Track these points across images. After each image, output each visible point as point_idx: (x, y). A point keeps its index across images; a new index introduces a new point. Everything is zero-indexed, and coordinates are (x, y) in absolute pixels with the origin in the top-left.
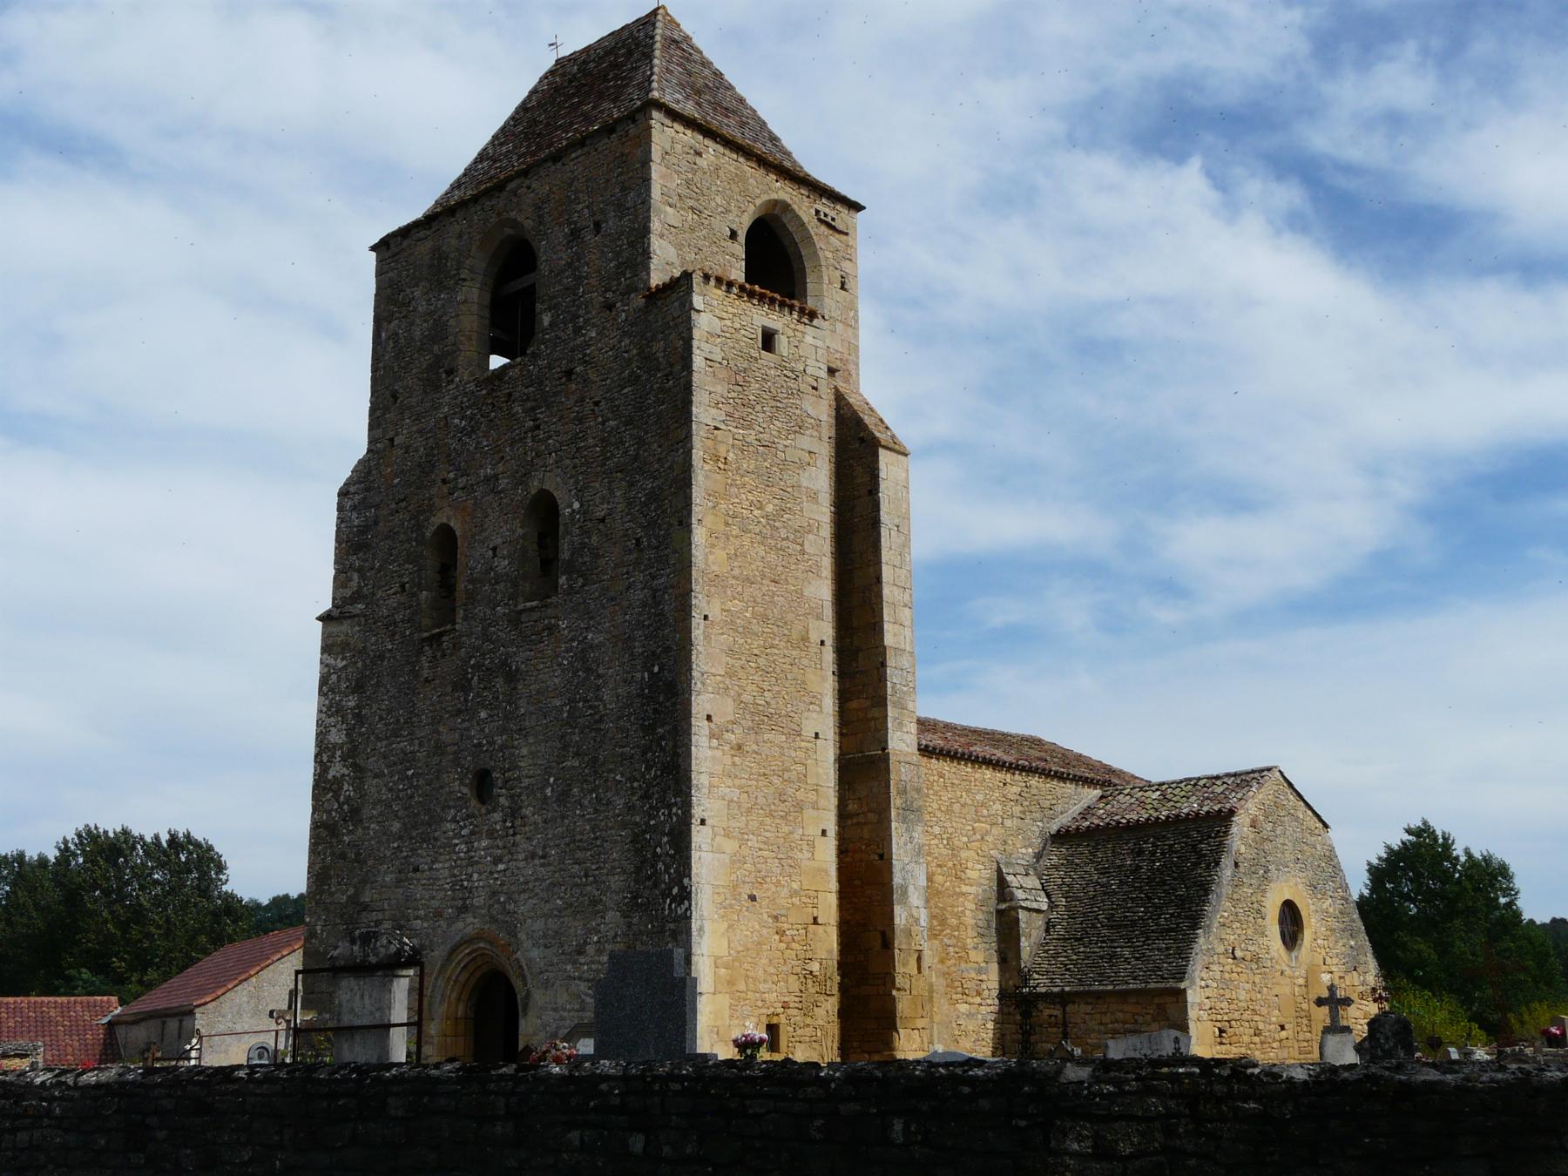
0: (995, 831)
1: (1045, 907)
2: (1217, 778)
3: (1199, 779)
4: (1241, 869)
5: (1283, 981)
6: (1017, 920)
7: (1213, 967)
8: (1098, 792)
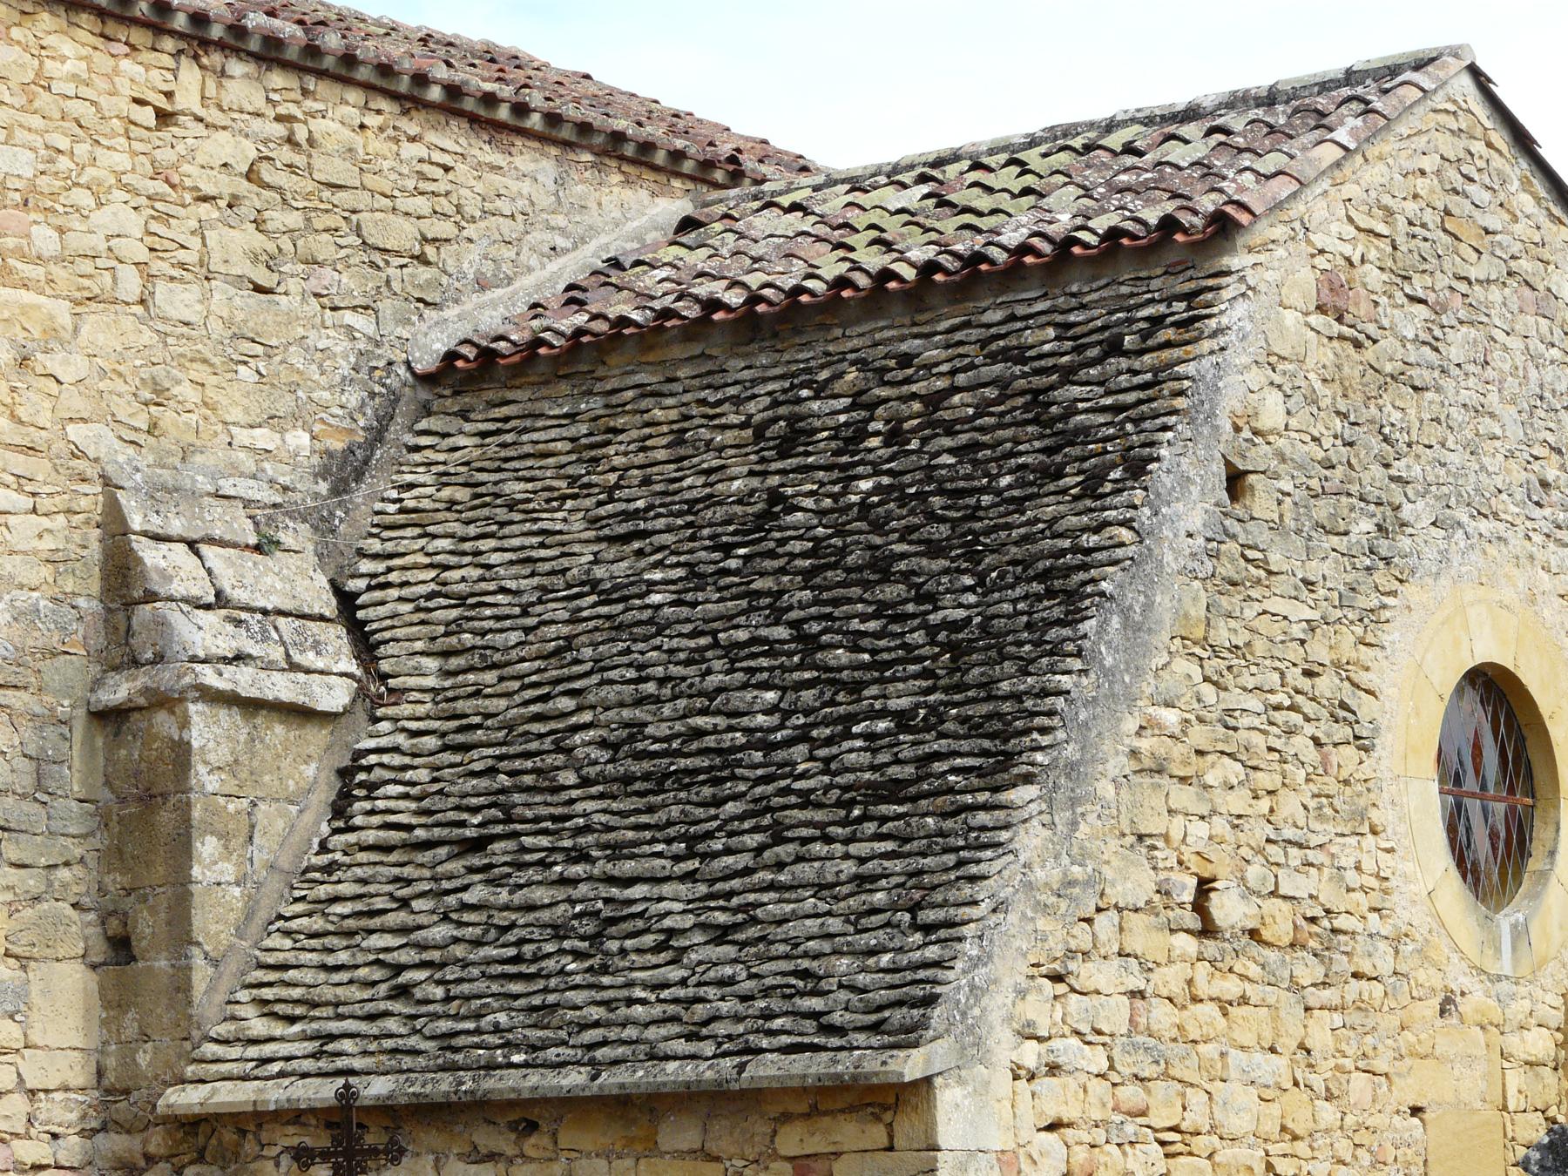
0: (99, 330)
1: (334, 696)
2: (1191, 114)
3: (1111, 126)
4: (1262, 501)
5: (1449, 1039)
6: (181, 754)
7: (1087, 973)
8: (675, 205)
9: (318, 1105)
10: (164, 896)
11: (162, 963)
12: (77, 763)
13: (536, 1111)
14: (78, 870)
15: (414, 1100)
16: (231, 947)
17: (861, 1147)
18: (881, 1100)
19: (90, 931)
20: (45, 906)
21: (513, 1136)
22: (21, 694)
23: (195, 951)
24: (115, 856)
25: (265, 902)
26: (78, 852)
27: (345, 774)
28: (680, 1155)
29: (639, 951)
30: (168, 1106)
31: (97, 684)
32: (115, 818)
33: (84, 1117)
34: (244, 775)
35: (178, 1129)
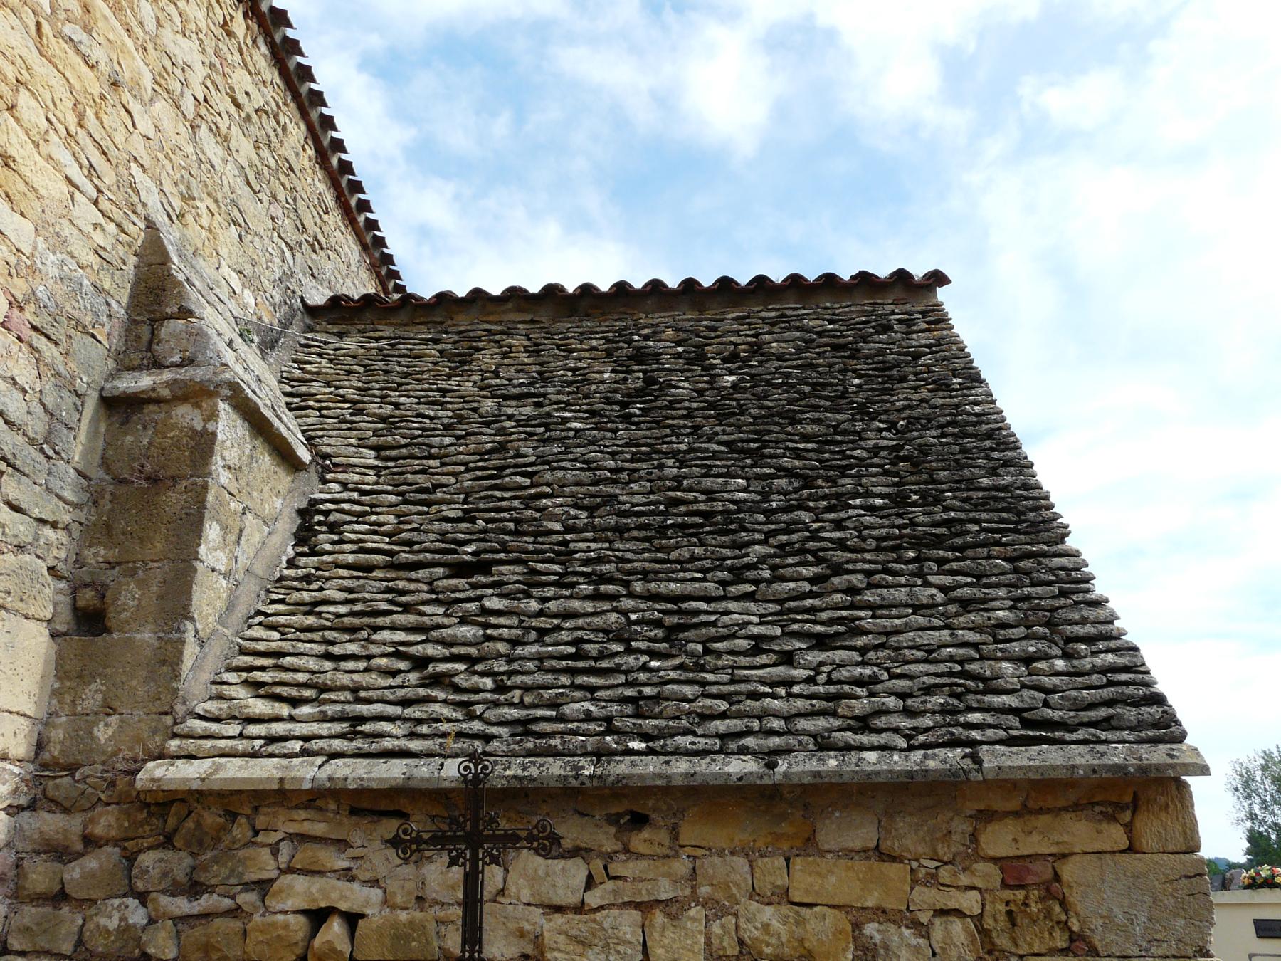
9: (375, 786)
10: (159, 573)
11: (146, 636)
12: (82, 436)
13: (650, 803)
14: (61, 536)
15: (516, 784)
16: (214, 631)
17: (1098, 847)
18: (1114, 799)
19: (61, 598)
20: (27, 558)
21: (613, 830)
22: (52, 346)
23: (189, 626)
24: (98, 529)
25: (243, 599)
26: (67, 518)
27: (304, 514)
28: (849, 853)
29: (732, 653)
30: (153, 780)
31: (112, 376)
32: (108, 496)
33: (16, 791)
34: (243, 483)
35: (141, 810)
